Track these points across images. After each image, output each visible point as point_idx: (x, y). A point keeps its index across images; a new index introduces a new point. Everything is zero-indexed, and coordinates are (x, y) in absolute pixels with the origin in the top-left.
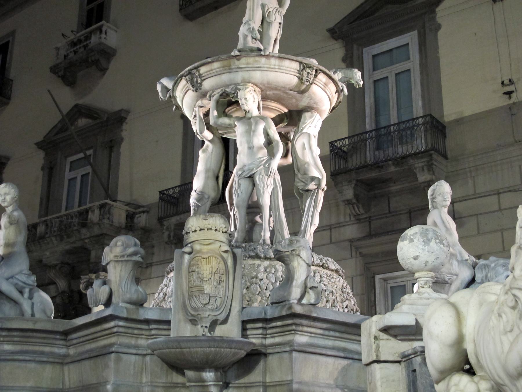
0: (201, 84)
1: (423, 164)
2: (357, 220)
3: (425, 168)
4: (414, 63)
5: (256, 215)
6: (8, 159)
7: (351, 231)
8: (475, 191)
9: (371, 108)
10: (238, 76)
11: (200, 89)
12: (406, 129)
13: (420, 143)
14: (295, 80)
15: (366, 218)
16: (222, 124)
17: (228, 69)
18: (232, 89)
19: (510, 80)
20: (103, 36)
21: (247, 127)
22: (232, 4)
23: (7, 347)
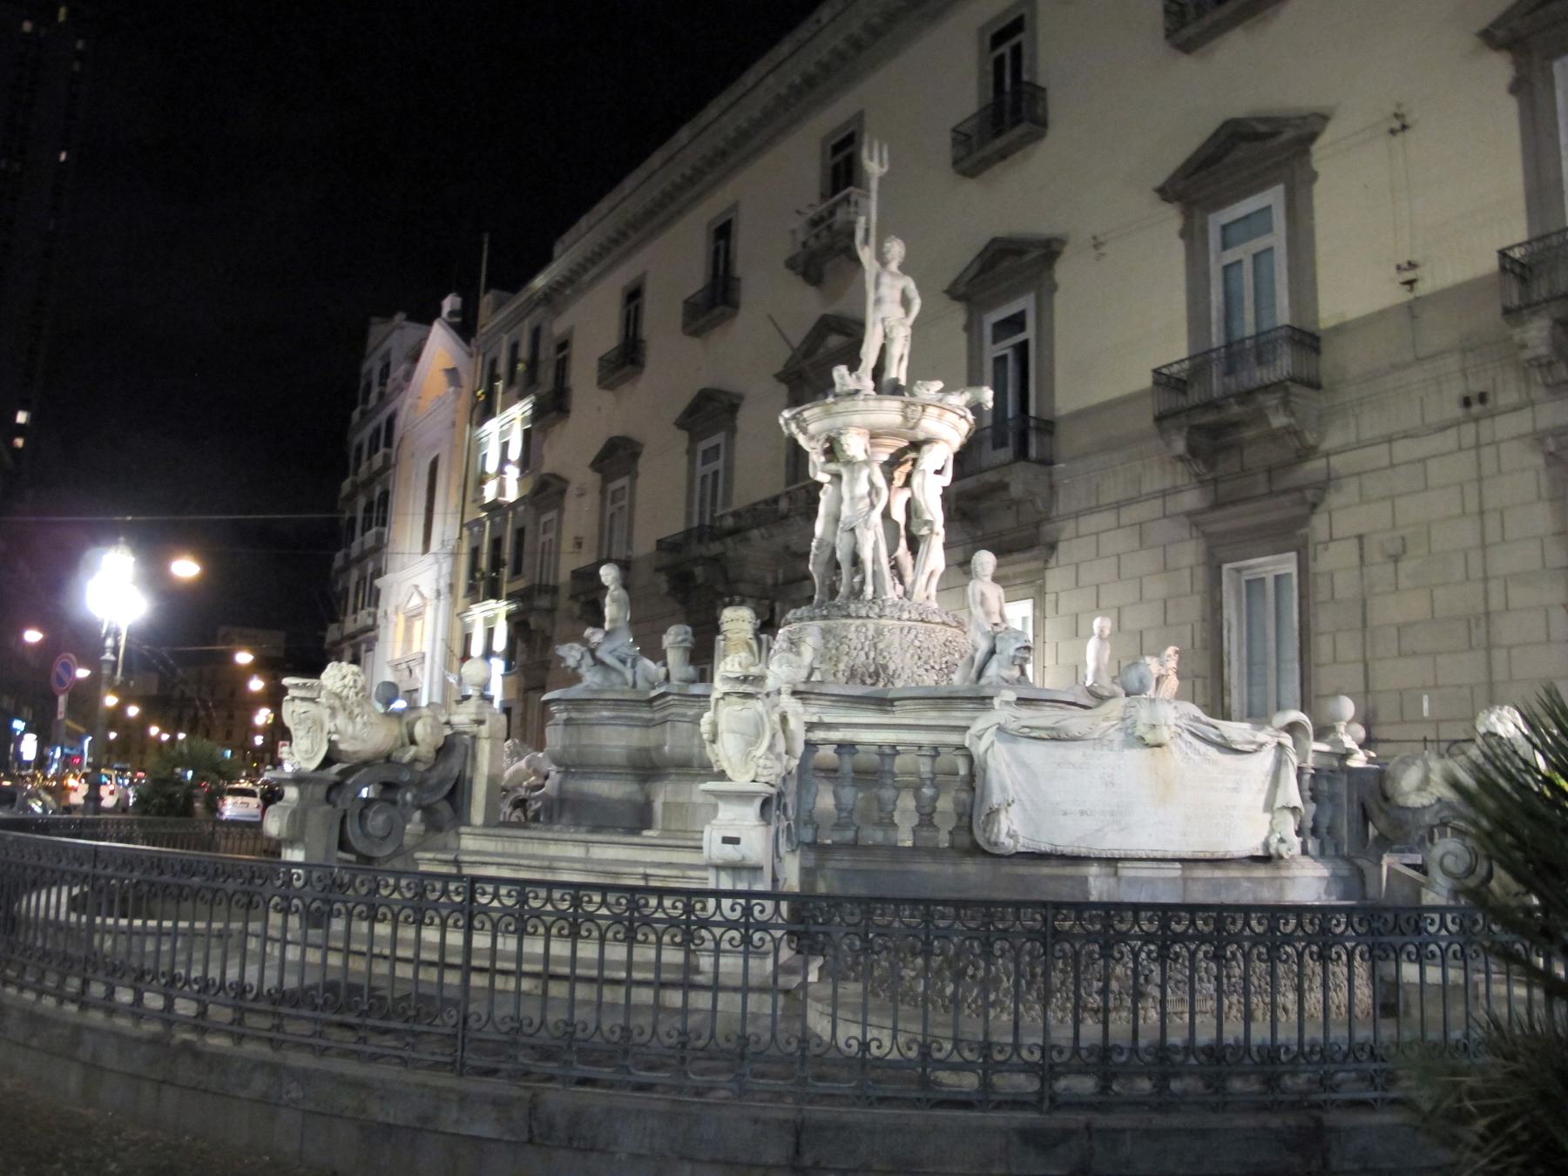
4: (1278, 239)
6: (741, 397)
7: (1191, 499)
10: (839, 421)
12: (1263, 346)
13: (1284, 364)
14: (898, 419)
17: (828, 414)
20: (852, 209)
22: (1029, 148)
23: (606, 714)
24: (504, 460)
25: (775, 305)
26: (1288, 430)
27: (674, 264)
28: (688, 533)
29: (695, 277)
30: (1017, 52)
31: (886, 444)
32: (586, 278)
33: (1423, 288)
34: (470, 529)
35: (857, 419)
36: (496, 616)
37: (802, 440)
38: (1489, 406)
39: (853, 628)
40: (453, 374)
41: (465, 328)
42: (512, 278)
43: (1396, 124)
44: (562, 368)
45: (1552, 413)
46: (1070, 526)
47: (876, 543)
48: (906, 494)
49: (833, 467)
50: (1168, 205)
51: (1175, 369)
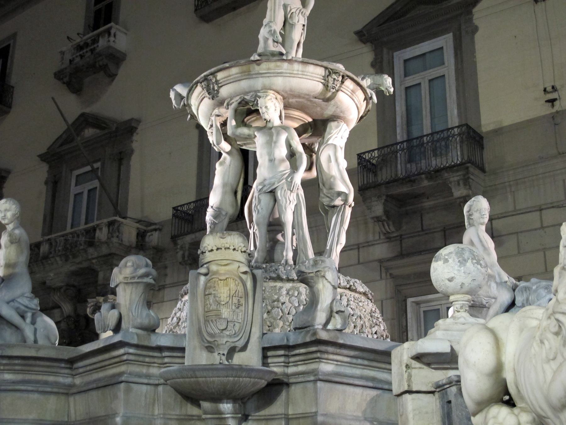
0: (218, 91)
1: (458, 178)
2: (387, 238)
3: (461, 182)
4: (449, 68)
5: (278, 234)
6: (9, 172)
7: (381, 251)
8: (515, 207)
9: (402, 117)
10: (259, 83)
11: (217, 97)
12: (440, 140)
13: (456, 155)
14: (319, 87)
15: (397, 236)
16: (241, 134)
17: (248, 75)
18: (252, 96)
19: (553, 87)
20: (112, 39)
21: (268, 138)
22: (252, 5)
23: (8, 376)
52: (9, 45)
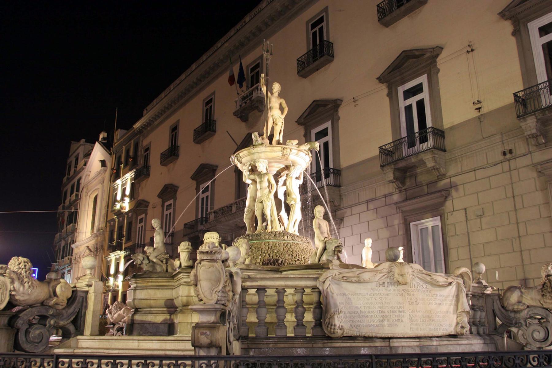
6: (217, 167)
7: (396, 197)
19: (478, 101)
22: (327, 66)
24: (124, 195)
25: (228, 124)
26: (434, 168)
27: (190, 116)
28: (197, 220)
29: (198, 121)
30: (321, 30)
31: (276, 167)
32: (156, 123)
33: (484, 110)
34: (110, 223)
35: (262, 155)
36: (120, 257)
37: (239, 166)
38: (513, 154)
39: (263, 244)
40: (103, 163)
41: (108, 145)
42: (127, 125)
43: (470, 49)
44: (147, 158)
45: (539, 156)
46: (348, 211)
47: (272, 207)
48: (284, 188)
49: (252, 177)
50: (382, 85)
51: (388, 146)
52: (323, 17)
